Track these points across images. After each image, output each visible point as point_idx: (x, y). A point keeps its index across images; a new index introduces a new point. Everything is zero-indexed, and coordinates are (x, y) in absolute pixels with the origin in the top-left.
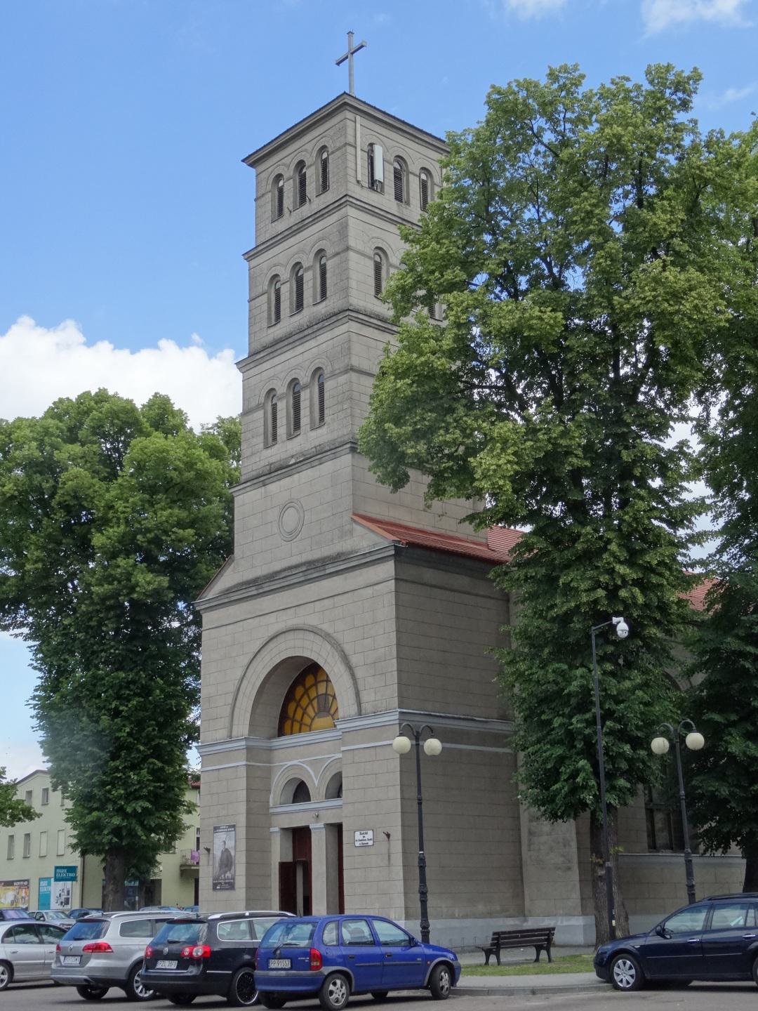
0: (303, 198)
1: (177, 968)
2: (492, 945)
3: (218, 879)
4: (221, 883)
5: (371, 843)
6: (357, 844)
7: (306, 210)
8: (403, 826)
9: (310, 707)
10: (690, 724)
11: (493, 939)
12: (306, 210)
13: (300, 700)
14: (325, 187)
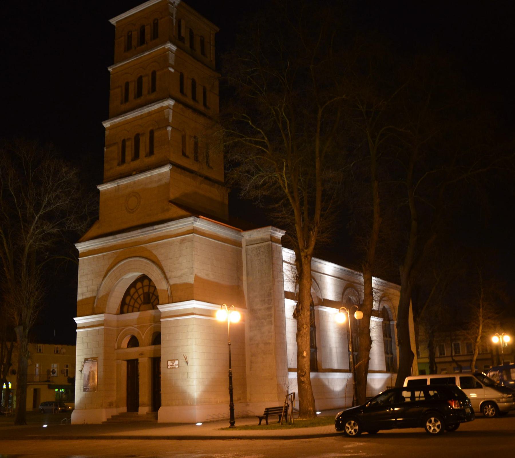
0: (136, 156)
1: (165, 47)
2: (264, 414)
3: (87, 386)
4: (88, 388)
5: (177, 367)
6: (169, 367)
7: (137, 164)
8: (172, 303)
9: (139, 299)
10: (357, 308)
11: (265, 412)
12: (137, 164)
13: (133, 295)
14: (151, 152)
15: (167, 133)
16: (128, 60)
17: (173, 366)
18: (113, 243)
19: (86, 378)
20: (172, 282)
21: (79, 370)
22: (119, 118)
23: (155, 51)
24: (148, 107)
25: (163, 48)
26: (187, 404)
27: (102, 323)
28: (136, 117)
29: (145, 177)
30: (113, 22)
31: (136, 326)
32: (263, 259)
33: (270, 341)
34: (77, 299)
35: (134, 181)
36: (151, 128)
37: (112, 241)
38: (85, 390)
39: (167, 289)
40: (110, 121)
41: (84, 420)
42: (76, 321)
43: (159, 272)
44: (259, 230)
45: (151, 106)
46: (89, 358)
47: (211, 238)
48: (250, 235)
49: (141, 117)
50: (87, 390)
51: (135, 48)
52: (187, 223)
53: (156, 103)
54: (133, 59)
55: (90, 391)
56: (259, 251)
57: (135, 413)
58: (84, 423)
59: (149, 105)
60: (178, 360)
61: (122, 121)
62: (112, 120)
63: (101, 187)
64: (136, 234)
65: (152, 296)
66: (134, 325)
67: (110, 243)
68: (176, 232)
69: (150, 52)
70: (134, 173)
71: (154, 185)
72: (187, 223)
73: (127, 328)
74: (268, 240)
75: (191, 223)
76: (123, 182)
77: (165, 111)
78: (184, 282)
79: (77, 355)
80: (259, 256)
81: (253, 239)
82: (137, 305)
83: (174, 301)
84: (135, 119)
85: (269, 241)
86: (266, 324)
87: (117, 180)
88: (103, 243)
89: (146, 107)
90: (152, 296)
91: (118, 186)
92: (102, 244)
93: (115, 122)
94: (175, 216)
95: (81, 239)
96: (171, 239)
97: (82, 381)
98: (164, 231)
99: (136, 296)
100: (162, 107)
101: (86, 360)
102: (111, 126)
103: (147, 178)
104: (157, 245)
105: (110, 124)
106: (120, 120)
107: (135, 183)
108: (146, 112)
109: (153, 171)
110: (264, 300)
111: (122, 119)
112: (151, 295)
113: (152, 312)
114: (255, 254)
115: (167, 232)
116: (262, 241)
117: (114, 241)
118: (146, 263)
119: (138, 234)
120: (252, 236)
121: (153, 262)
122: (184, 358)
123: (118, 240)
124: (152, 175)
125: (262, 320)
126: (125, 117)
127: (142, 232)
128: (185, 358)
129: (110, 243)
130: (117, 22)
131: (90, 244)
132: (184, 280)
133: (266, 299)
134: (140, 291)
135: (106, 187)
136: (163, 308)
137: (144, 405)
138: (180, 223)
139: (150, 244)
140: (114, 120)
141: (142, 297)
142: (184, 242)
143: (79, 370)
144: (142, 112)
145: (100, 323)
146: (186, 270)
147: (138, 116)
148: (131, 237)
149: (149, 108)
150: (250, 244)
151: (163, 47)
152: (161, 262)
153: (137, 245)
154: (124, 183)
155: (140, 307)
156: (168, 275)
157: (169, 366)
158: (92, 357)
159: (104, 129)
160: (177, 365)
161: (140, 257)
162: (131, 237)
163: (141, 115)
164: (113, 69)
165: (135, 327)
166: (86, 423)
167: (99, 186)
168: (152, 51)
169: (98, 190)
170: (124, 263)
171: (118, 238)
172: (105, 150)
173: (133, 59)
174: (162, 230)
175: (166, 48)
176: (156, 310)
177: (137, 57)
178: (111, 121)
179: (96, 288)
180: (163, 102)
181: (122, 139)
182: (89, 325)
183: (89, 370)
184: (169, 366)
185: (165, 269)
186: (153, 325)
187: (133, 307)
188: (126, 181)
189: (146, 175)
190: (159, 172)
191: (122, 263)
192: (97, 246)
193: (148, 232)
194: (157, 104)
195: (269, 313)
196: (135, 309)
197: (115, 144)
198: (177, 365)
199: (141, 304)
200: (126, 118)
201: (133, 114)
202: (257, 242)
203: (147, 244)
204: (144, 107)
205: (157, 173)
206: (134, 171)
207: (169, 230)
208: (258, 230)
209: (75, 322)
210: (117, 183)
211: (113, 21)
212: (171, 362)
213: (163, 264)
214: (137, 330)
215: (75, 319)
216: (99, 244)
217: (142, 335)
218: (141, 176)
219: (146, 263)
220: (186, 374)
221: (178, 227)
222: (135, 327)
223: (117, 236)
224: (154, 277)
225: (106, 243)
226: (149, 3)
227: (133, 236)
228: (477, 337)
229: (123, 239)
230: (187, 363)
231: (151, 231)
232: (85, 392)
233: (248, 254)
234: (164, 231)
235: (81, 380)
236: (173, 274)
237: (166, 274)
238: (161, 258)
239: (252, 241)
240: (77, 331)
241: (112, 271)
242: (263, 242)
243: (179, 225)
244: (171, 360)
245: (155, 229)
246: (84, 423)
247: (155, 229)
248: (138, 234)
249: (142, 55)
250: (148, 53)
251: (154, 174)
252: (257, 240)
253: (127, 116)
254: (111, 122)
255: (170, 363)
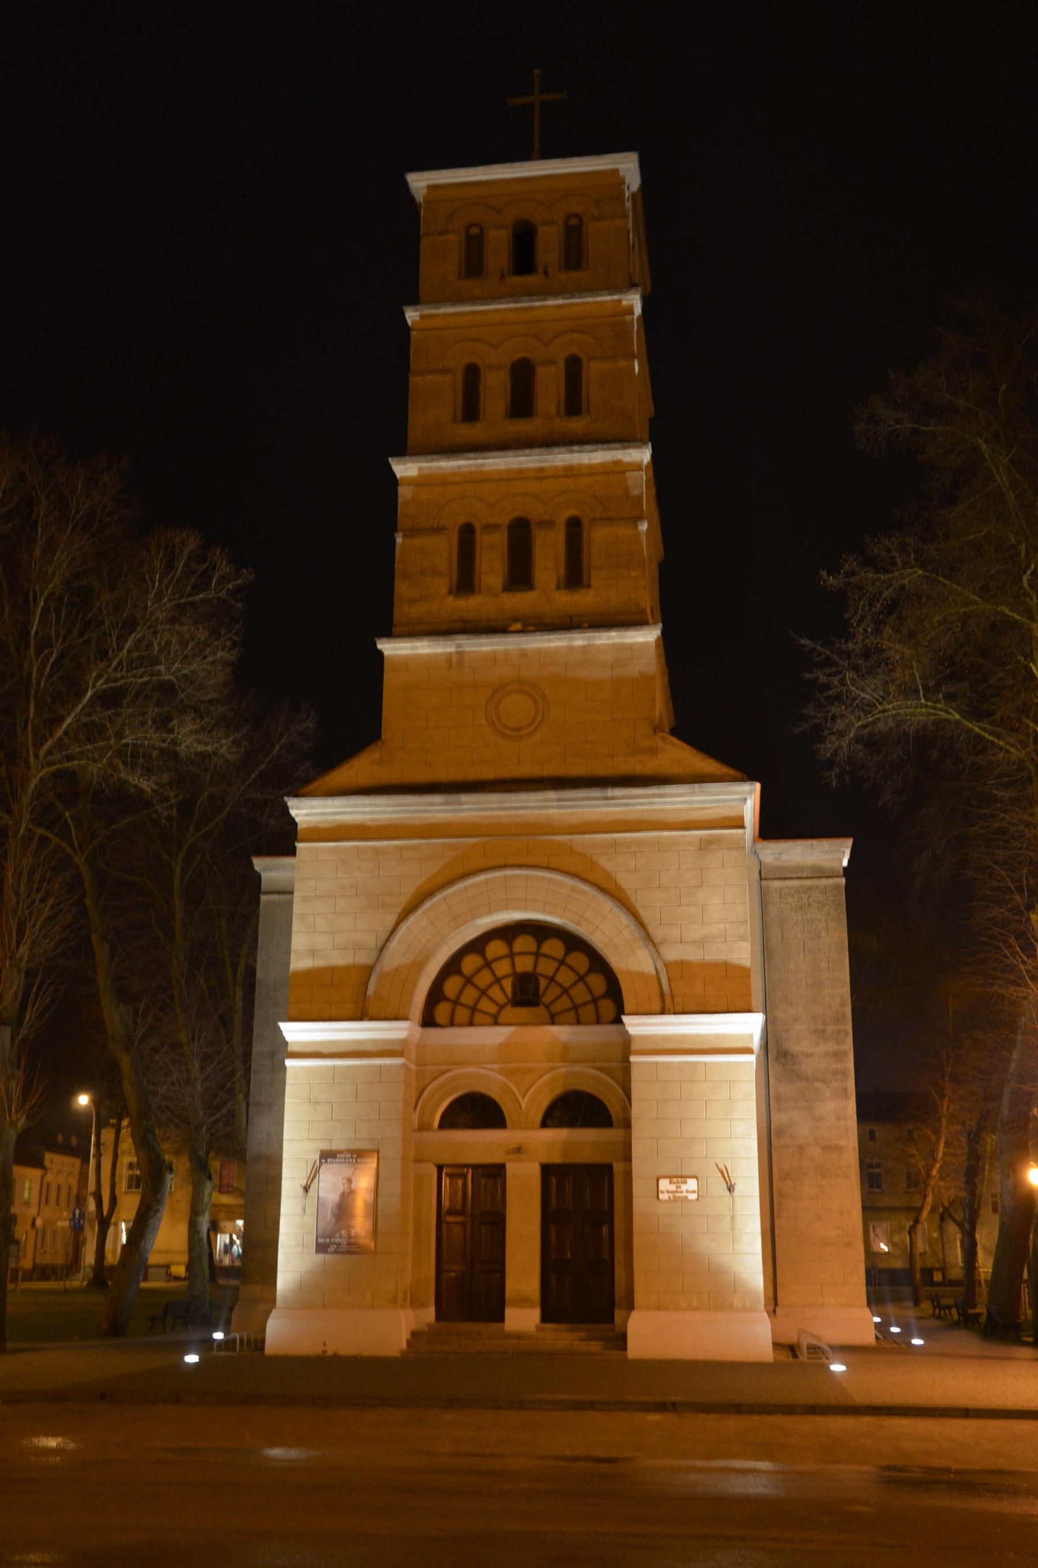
5: (693, 1197)
6: (663, 1197)
15: (637, 536)
16: (482, 304)
17: (677, 1195)
18: (440, 815)
19: (329, 1211)
20: (672, 953)
21: (301, 1186)
22: (458, 459)
23: (584, 304)
24: (572, 452)
25: (612, 301)
26: (731, 1308)
27: (397, 1047)
28: (521, 471)
29: (564, 644)
30: (417, 181)
31: (496, 1066)
32: (819, 921)
33: (843, 1143)
34: (289, 964)
35: (522, 650)
36: (572, 512)
37: (439, 811)
38: (321, 1248)
39: (654, 972)
40: (420, 461)
41: (325, 1344)
42: (285, 1034)
43: (624, 919)
44: (812, 845)
45: (580, 452)
46: (340, 1152)
47: (411, 837)
48: (780, 854)
49: (540, 475)
50: (332, 1248)
51: (503, 276)
52: (721, 797)
53: (600, 446)
54: (503, 306)
55: (342, 1253)
56: (805, 900)
57: (494, 1326)
58: (325, 1352)
59: (575, 448)
60: (696, 1178)
61: (466, 470)
62: (432, 461)
63: (392, 645)
64: (538, 801)
65: (547, 988)
66: (486, 1063)
67: (429, 815)
68: (684, 817)
69: (568, 301)
70: (518, 626)
71: (604, 674)
72: (721, 797)
73: (458, 1071)
74: (836, 874)
75: (739, 800)
76: (481, 645)
77: (628, 474)
78: (712, 958)
79: (285, 1137)
80: (806, 914)
81: (786, 865)
82: (485, 1005)
83: (679, 1009)
84: (519, 475)
85: (837, 876)
86: (828, 1094)
87: (460, 637)
88: (401, 812)
89: (563, 449)
90: (547, 988)
91: (458, 653)
92: (394, 812)
93: (439, 468)
94: (676, 770)
95: (311, 787)
96: (666, 833)
97: (310, 1221)
98: (638, 808)
99: (484, 979)
100: (617, 463)
101: (327, 1156)
102: (419, 476)
103: (571, 649)
104: (615, 844)
105: (420, 469)
106: (459, 467)
107: (524, 654)
108: (560, 464)
109: (598, 634)
110: (823, 1031)
111: (468, 466)
112: (543, 983)
113: (604, 1033)
114: (793, 905)
115: (654, 811)
116: (816, 875)
117: (446, 811)
118: (573, 889)
119: (545, 804)
120: (784, 857)
121: (603, 890)
122: (720, 1175)
123: (463, 810)
124: (592, 642)
125: (818, 1084)
126: (480, 461)
127: (558, 800)
128: (724, 1174)
129: (429, 815)
130: (431, 188)
131: (349, 806)
132: (715, 954)
133: (830, 1028)
134: (503, 968)
135: (413, 648)
136: (636, 1026)
137: (523, 1302)
138: (701, 793)
139: (587, 836)
140: (438, 460)
141: (508, 984)
142: (714, 846)
143: (301, 1186)
144: (544, 462)
145: (389, 1047)
146: (721, 926)
147: (529, 470)
148: (516, 808)
149: (574, 455)
150: (777, 876)
151: (616, 297)
152: (628, 893)
153: (538, 835)
154: (484, 649)
155: (549, 1011)
156: (658, 933)
157: (662, 1192)
158: (352, 1147)
159: (393, 481)
160: (694, 1192)
161: (549, 868)
162: (516, 808)
163: (541, 470)
164: (422, 317)
165: (491, 1070)
166: (330, 1352)
167: (385, 640)
168: (573, 301)
169: (380, 654)
170: (486, 881)
171: (467, 803)
172: (399, 540)
173: (503, 306)
174: (634, 804)
175: (624, 303)
176: (620, 1026)
177: (517, 302)
178: (428, 461)
179: (372, 941)
180: (624, 448)
181: (463, 520)
182: (342, 1049)
183: (341, 1188)
184: (662, 1192)
185: (643, 914)
186: (563, 1070)
187: (474, 1009)
188: (491, 644)
189: (570, 639)
190: (618, 640)
191: (481, 878)
192: (375, 816)
193: (581, 803)
194: (603, 449)
195: (839, 1066)
196: (478, 1017)
197: (440, 529)
198: (694, 1192)
199: (505, 1005)
200: (483, 465)
201: (511, 459)
202: (799, 875)
203: (577, 837)
204: (556, 450)
205: (610, 641)
206: (517, 620)
207: (656, 807)
208: (810, 842)
209: (284, 1038)
210: (458, 646)
211: (419, 182)
212: (670, 1183)
213: (639, 901)
214: (501, 1078)
215: (284, 1026)
216: (387, 812)
217: (520, 1098)
218: (550, 641)
219: (573, 889)
220: (728, 1219)
221: (692, 802)
222: (491, 1070)
223: (465, 798)
224: (604, 932)
225: (415, 812)
226: (560, 166)
227: (525, 804)
228: (933, 1166)
229: (481, 810)
230: (731, 1188)
231: (594, 802)
232: (321, 1257)
233: (772, 904)
234: (638, 808)
235: (305, 1218)
236: (675, 932)
237: (650, 929)
238: (626, 881)
239: (781, 869)
240: (289, 1063)
241: (439, 897)
242: (819, 878)
243: (696, 798)
244: (670, 1177)
245: (613, 798)
246: (325, 1352)
247: (613, 798)
248: (545, 804)
249: (538, 304)
250: (560, 302)
251: (600, 642)
252: (802, 868)
253: (490, 461)
254: (424, 465)
255: (664, 1184)
